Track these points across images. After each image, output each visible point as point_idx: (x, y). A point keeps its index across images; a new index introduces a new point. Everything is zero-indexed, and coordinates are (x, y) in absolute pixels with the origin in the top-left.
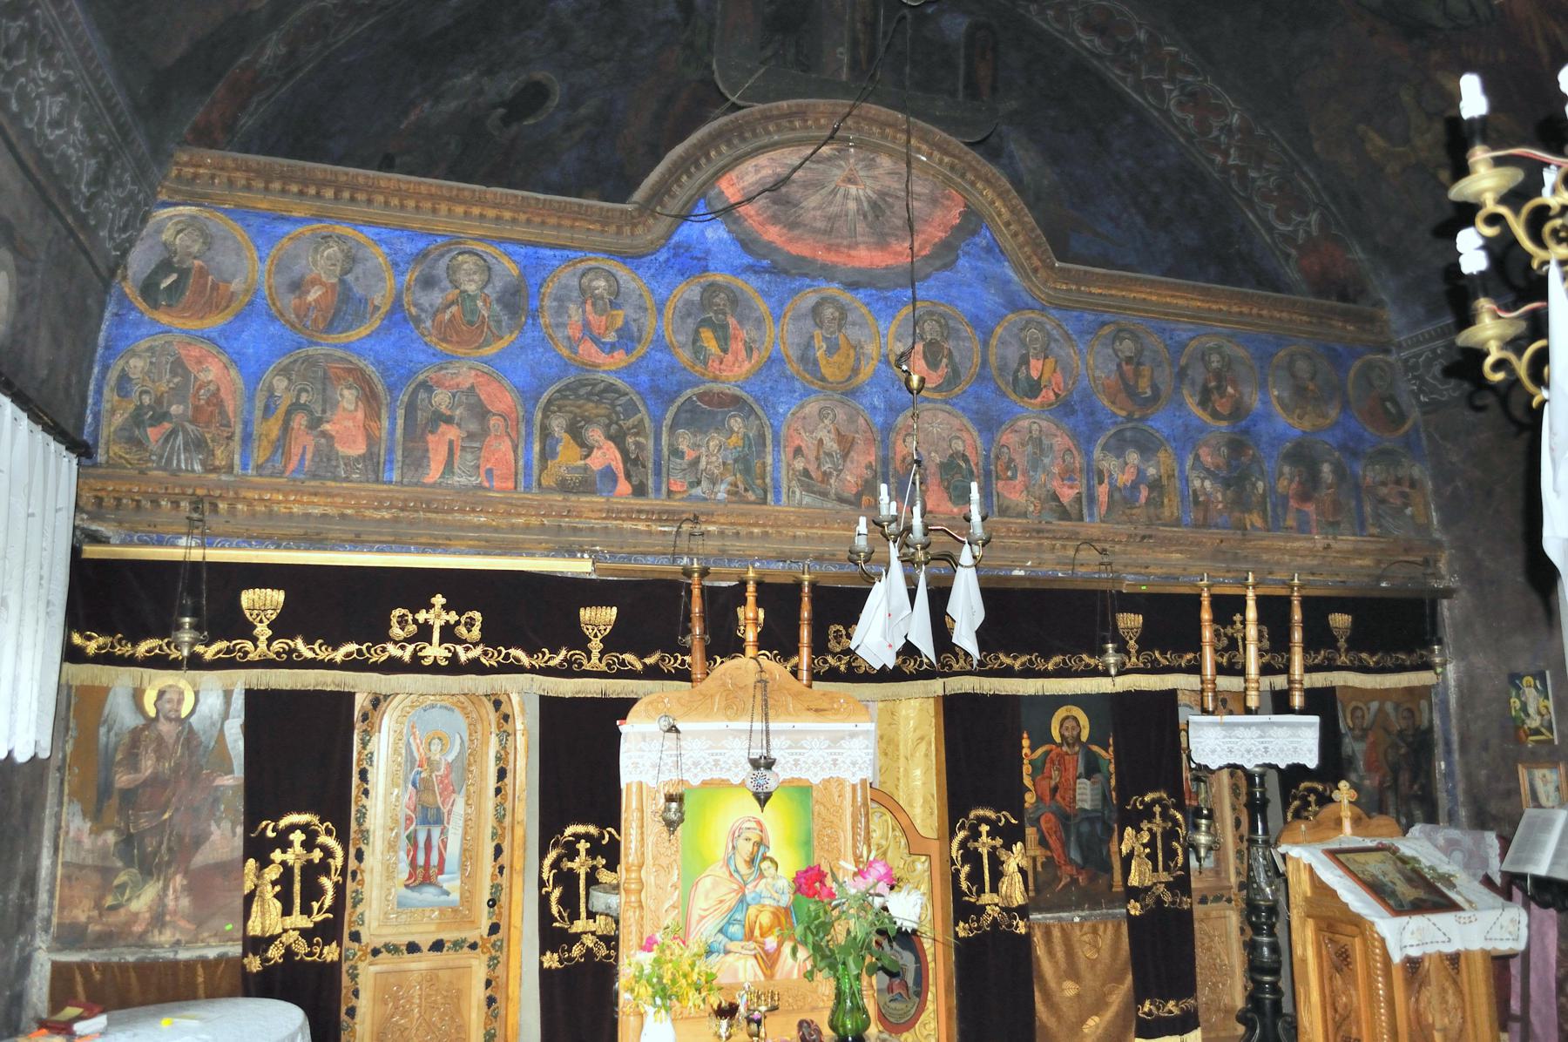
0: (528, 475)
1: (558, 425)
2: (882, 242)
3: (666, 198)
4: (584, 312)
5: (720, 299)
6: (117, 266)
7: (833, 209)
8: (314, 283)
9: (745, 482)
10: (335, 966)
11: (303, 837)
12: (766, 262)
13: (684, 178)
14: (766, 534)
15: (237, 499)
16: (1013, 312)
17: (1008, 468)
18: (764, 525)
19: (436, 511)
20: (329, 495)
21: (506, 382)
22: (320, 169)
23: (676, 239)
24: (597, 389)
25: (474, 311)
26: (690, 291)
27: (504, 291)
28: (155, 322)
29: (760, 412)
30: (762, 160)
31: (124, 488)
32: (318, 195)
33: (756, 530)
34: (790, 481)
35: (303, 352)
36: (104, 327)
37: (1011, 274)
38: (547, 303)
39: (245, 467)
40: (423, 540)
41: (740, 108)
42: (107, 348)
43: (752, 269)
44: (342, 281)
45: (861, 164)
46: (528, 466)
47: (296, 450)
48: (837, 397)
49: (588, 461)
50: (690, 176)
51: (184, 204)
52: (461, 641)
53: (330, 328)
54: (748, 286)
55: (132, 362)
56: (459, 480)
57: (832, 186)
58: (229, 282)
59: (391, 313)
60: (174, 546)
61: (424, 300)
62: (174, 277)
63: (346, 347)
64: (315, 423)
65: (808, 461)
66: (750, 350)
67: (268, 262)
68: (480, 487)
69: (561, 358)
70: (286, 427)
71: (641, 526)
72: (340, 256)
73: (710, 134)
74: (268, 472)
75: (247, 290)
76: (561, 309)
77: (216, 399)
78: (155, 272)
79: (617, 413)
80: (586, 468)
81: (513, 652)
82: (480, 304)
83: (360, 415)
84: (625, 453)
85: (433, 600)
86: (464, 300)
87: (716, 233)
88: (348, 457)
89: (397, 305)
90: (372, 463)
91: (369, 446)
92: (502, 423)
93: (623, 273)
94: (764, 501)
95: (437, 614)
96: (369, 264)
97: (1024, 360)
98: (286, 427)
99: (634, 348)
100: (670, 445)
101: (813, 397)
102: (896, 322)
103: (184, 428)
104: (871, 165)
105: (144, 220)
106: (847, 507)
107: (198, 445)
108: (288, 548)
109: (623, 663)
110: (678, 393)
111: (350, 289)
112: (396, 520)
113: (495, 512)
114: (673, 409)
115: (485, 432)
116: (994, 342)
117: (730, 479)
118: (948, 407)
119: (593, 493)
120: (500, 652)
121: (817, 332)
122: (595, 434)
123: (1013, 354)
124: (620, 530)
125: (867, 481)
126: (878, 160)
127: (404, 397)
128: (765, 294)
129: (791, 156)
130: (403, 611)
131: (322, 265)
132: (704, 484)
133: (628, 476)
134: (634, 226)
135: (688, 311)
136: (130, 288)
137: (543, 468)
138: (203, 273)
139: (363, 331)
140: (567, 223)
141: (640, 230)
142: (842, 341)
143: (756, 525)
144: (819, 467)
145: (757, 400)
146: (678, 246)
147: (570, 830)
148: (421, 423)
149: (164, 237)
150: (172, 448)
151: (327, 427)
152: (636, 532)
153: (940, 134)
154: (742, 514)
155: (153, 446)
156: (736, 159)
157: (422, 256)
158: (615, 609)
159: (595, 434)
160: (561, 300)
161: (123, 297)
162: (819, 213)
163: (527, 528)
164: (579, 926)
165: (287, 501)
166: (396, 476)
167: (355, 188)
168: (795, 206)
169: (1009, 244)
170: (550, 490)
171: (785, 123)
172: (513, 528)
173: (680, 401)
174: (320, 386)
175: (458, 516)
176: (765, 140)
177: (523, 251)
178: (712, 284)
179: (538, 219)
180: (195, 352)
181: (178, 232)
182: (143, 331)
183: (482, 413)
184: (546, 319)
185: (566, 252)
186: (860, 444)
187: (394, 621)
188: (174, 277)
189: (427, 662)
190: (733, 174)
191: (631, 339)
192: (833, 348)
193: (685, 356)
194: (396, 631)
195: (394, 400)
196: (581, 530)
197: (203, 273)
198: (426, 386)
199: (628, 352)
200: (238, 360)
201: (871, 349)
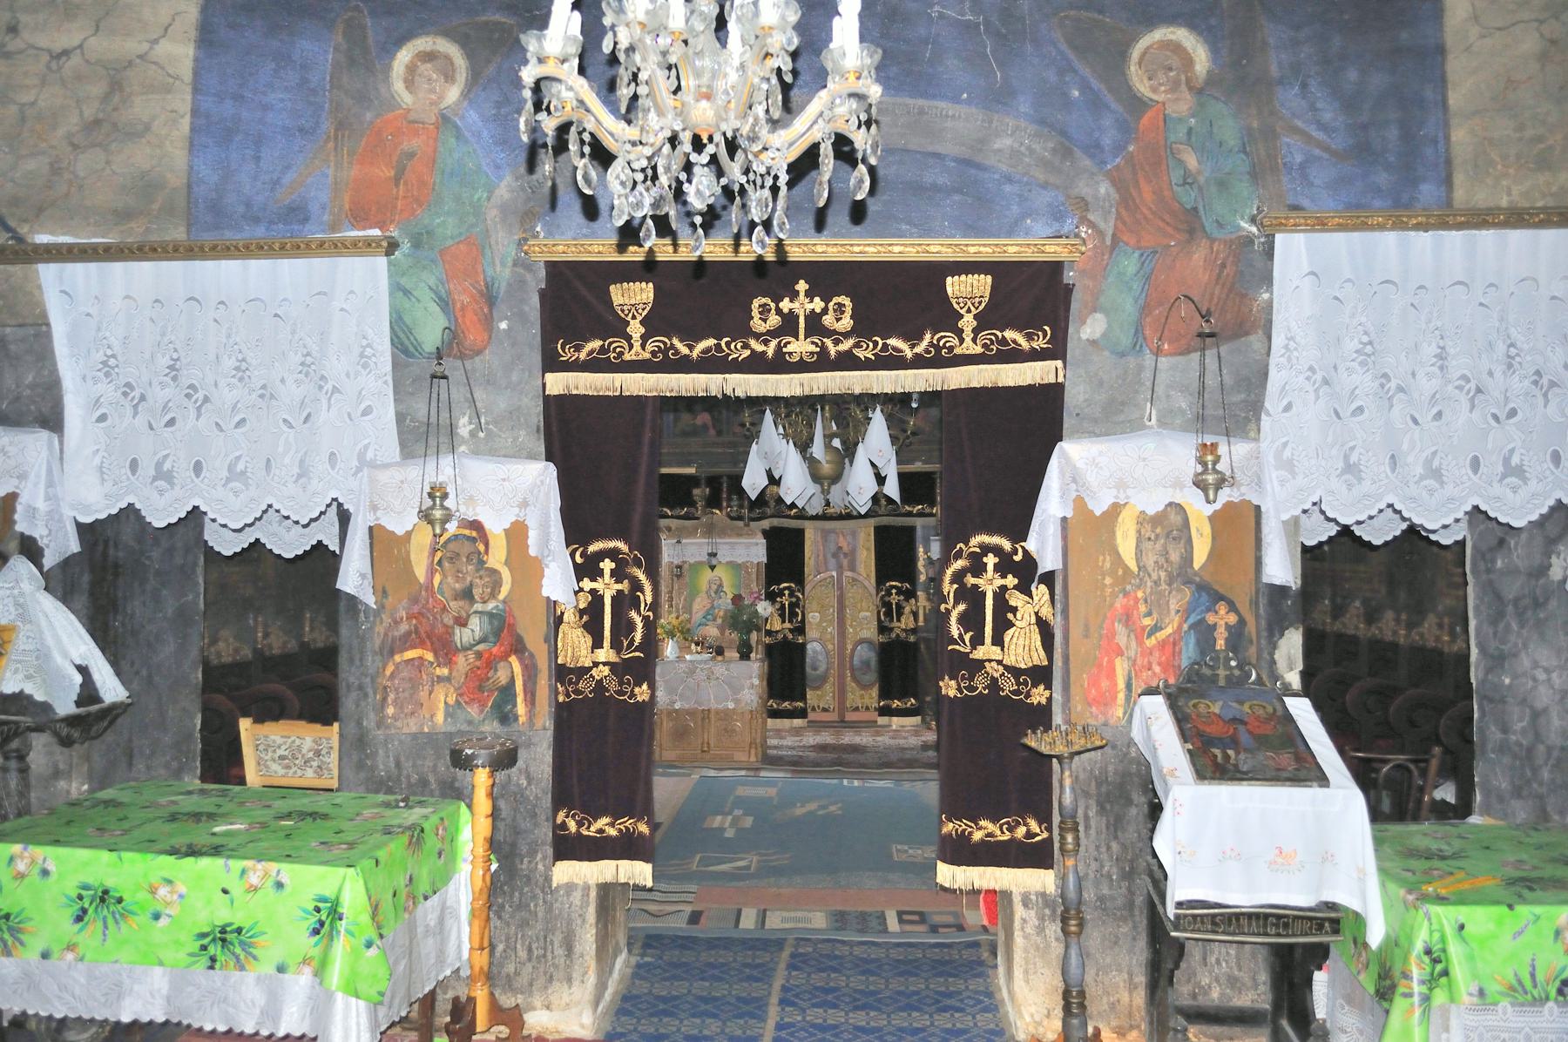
10: (771, 696)
11: (613, 565)
52: (829, 333)
81: (893, 342)
85: (817, 299)
95: (802, 305)
109: (1004, 341)
120: (876, 344)
130: (764, 300)
147: (977, 540)
164: (986, 651)
187: (755, 313)
189: (795, 359)
194: (757, 324)
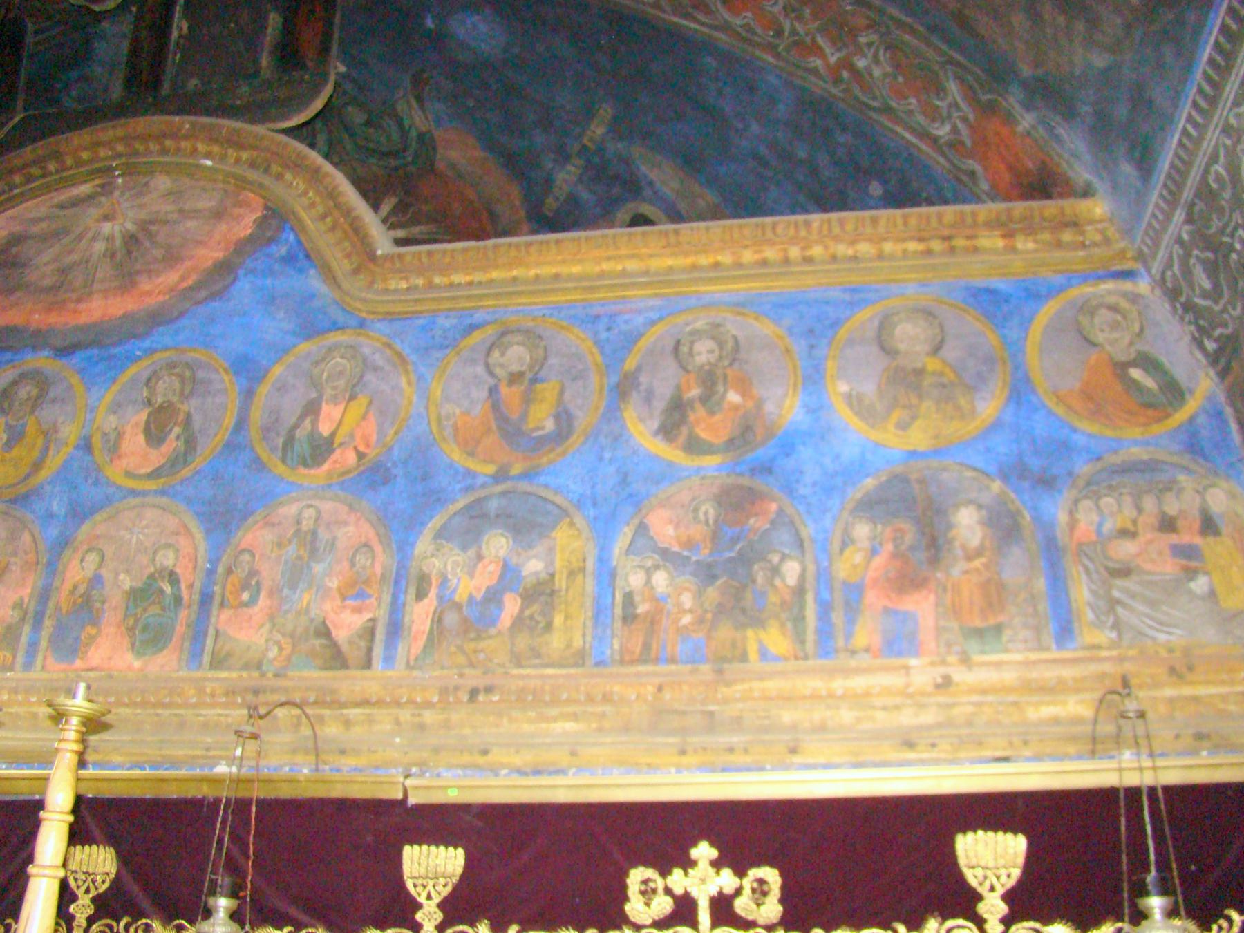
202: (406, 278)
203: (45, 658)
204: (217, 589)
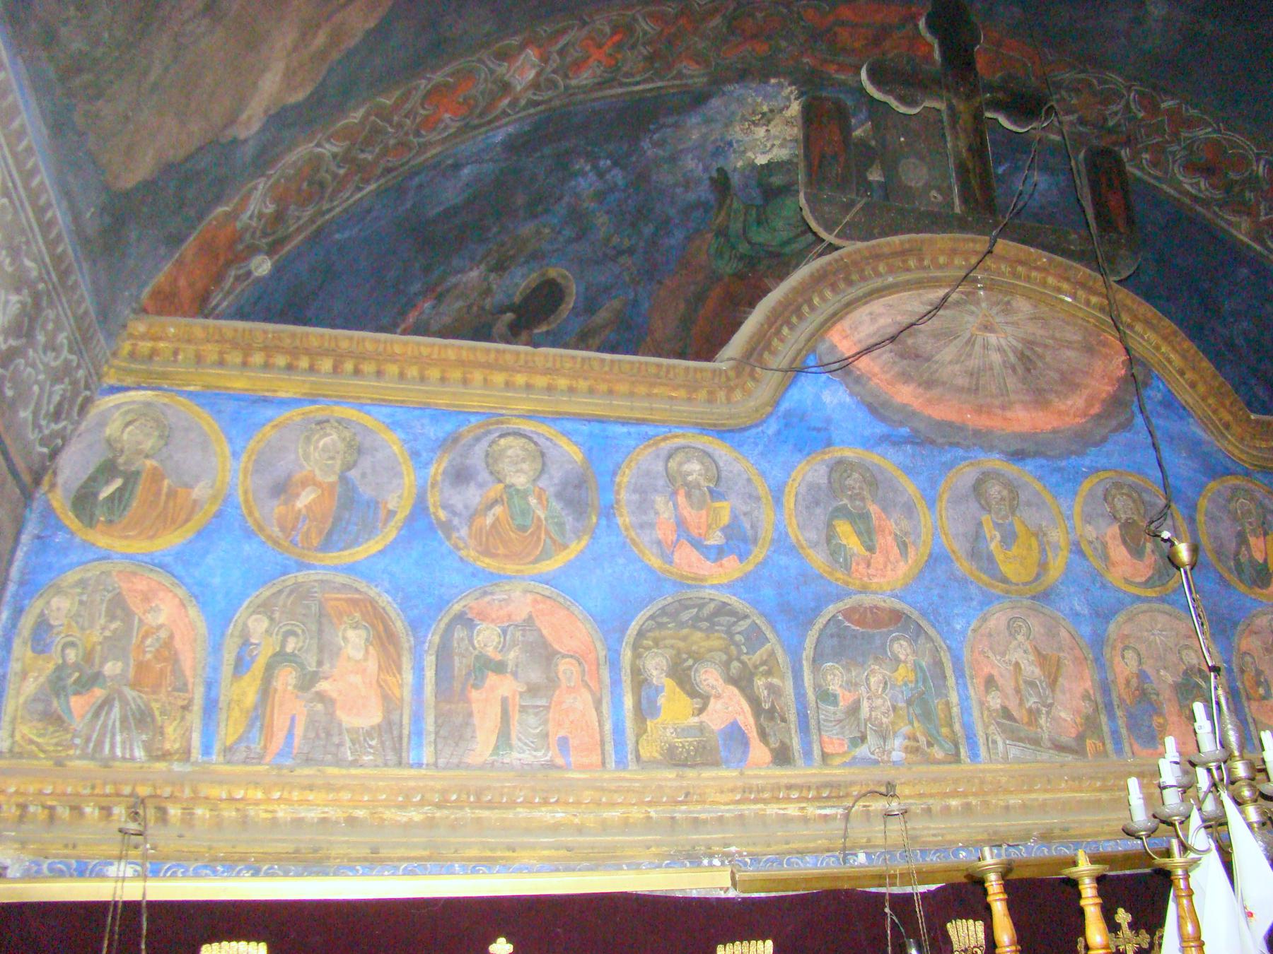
0: (619, 744)
1: (656, 666)
2: (1039, 398)
3: (766, 355)
4: (676, 506)
5: (854, 480)
6: (45, 469)
7: (973, 363)
8: (304, 484)
9: (927, 734)
12: (905, 431)
13: (785, 331)
14: (967, 806)
15: (196, 799)
16: (1214, 478)
17: (1258, 684)
18: (964, 794)
19: (490, 806)
20: (329, 787)
21: (577, 610)
22: (315, 335)
23: (785, 405)
24: (706, 612)
25: (526, 511)
26: (810, 472)
27: (564, 484)
28: (87, 545)
29: (932, 632)
30: (877, 306)
31: (32, 789)
32: (312, 369)
33: (954, 803)
34: (986, 726)
35: (290, 579)
36: (20, 554)
37: (1200, 432)
38: (624, 495)
39: (207, 750)
40: (474, 852)
41: (837, 248)
42: (22, 583)
43: (884, 439)
44: (343, 479)
45: (994, 311)
46: (618, 730)
47: (280, 723)
48: (1027, 602)
49: (704, 717)
50: (792, 328)
51: (139, 388)
53: (326, 546)
54: (886, 461)
55: (55, 602)
56: (520, 755)
57: (967, 335)
58: (189, 487)
59: (411, 519)
60: (101, 876)
61: (457, 500)
62: (118, 482)
63: (351, 569)
64: (307, 681)
65: (1006, 696)
66: (903, 547)
67: (244, 458)
68: (551, 766)
69: (650, 570)
70: (266, 691)
71: (792, 810)
72: (341, 446)
73: (812, 276)
74: (240, 755)
75: (214, 497)
76: (644, 505)
77: (168, 652)
78: (93, 478)
79: (737, 645)
80: (701, 729)
82: (533, 501)
83: (372, 665)
84: (754, 702)
86: (510, 497)
87: (830, 397)
88: (357, 730)
89: (420, 507)
90: (392, 738)
91: (387, 712)
92: (575, 669)
93: (722, 451)
94: (956, 758)
96: (379, 455)
97: (1242, 539)
98: (266, 691)
99: (749, 553)
100: (817, 686)
101: (996, 606)
102: (1079, 499)
103: (120, 693)
104: (1007, 309)
105: (83, 409)
106: (1069, 758)
107: (142, 719)
108: (270, 874)
110: (817, 611)
111: (354, 489)
112: (430, 823)
113: (578, 803)
114: (813, 634)
115: (552, 682)
116: (1201, 518)
117: (906, 729)
118: (1167, 607)
119: (716, 764)
121: (985, 518)
122: (709, 677)
123: (1226, 531)
124: (762, 819)
125: (1087, 718)
126: (1014, 303)
127: (434, 638)
128: (908, 471)
129: (911, 304)
131: (317, 459)
132: (871, 738)
133: (763, 735)
134: (731, 390)
135: (813, 498)
136: (59, 501)
137: (641, 731)
138: (157, 476)
139: (373, 546)
140: (642, 390)
141: (738, 395)
142: (1018, 528)
143: (954, 794)
144: (1021, 703)
145: (923, 614)
146: (788, 414)
148: (456, 677)
149: (108, 431)
150: (105, 725)
151: (323, 686)
152: (785, 820)
153: (1082, 271)
154: (934, 780)
155: (78, 724)
156: (848, 304)
157: (454, 439)
158: (769, 943)
159: (709, 677)
160: (643, 492)
161: (48, 513)
162: (957, 367)
163: (626, 825)
165: (269, 800)
166: (427, 755)
167: (362, 357)
168: (928, 359)
169: (1186, 397)
170: (654, 763)
171: (897, 262)
172: (605, 827)
173: (821, 622)
174: (314, 627)
175: (522, 812)
176: (878, 283)
177: (586, 428)
178: (840, 462)
179: (603, 387)
180: (141, 585)
181: (129, 423)
182: (74, 557)
183: (545, 654)
184: (624, 519)
185: (644, 429)
186: (1069, 666)
188: (118, 482)
190: (846, 323)
191: (745, 540)
192: (1009, 538)
193: (818, 559)
195: (420, 642)
196: (705, 822)
197: (157, 476)
198: (464, 620)
199: (742, 558)
200: (200, 595)
201: (1057, 536)
202: (1267, 441)
203: (1131, 745)
204: (1239, 684)
